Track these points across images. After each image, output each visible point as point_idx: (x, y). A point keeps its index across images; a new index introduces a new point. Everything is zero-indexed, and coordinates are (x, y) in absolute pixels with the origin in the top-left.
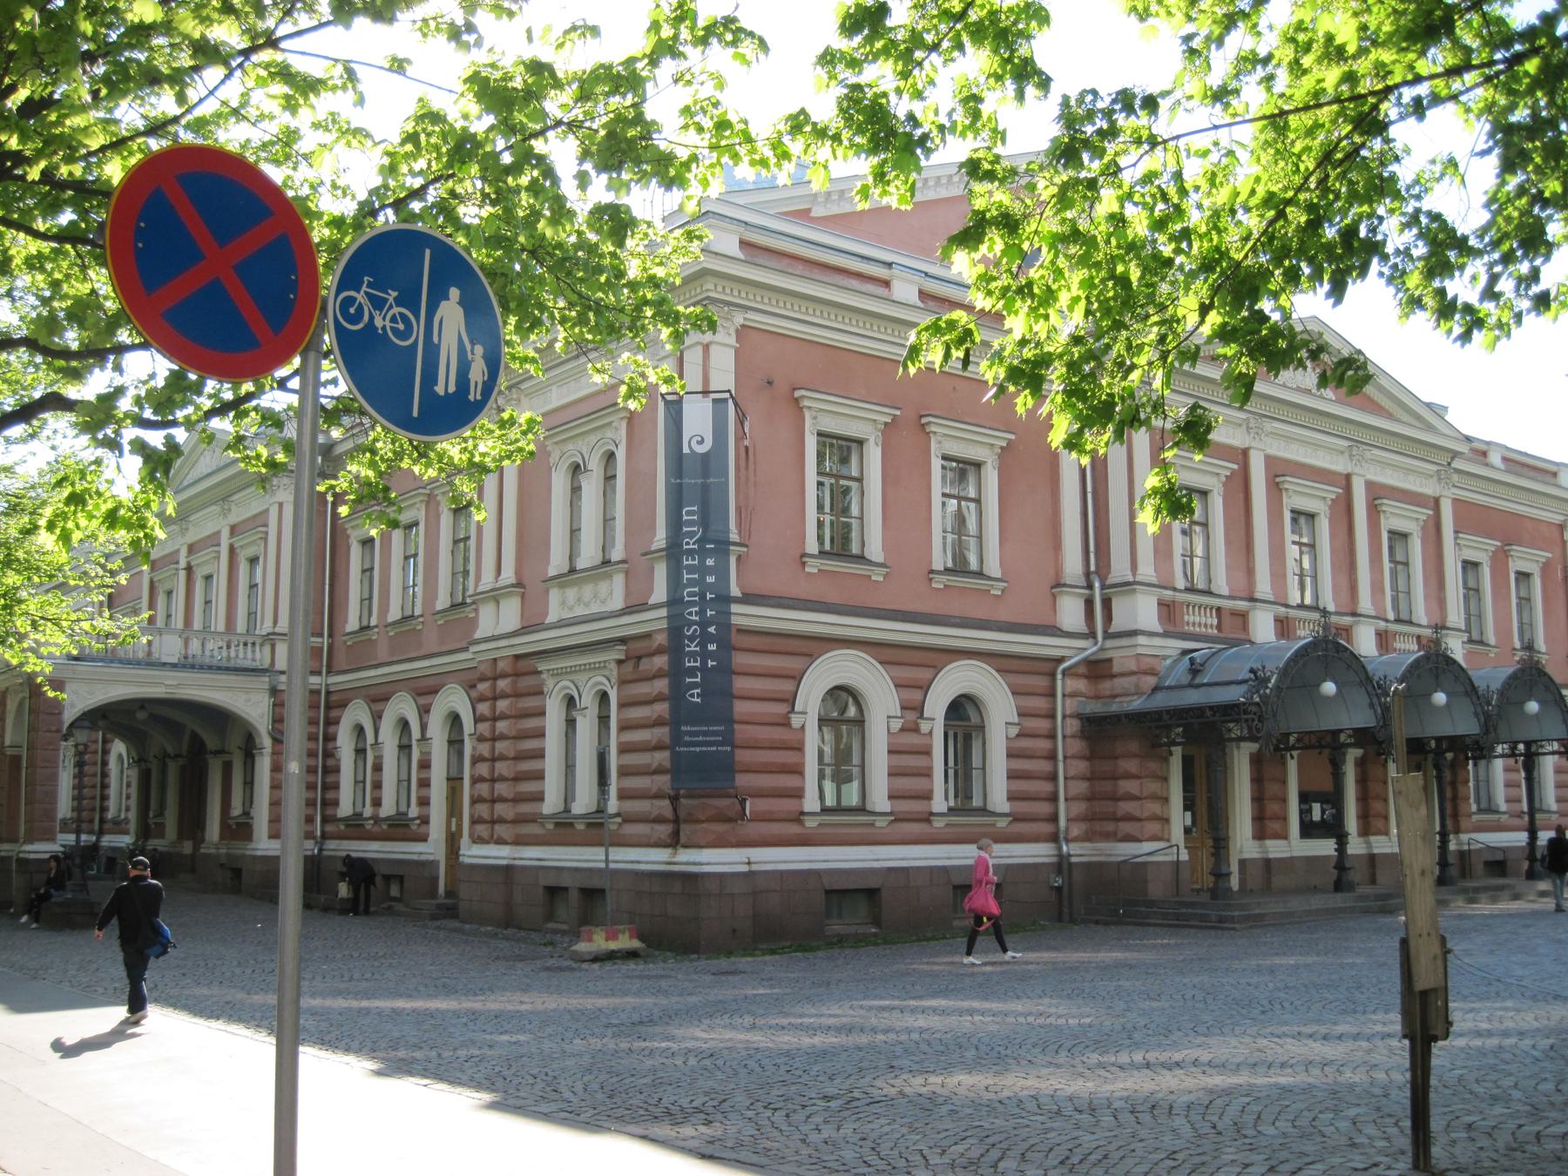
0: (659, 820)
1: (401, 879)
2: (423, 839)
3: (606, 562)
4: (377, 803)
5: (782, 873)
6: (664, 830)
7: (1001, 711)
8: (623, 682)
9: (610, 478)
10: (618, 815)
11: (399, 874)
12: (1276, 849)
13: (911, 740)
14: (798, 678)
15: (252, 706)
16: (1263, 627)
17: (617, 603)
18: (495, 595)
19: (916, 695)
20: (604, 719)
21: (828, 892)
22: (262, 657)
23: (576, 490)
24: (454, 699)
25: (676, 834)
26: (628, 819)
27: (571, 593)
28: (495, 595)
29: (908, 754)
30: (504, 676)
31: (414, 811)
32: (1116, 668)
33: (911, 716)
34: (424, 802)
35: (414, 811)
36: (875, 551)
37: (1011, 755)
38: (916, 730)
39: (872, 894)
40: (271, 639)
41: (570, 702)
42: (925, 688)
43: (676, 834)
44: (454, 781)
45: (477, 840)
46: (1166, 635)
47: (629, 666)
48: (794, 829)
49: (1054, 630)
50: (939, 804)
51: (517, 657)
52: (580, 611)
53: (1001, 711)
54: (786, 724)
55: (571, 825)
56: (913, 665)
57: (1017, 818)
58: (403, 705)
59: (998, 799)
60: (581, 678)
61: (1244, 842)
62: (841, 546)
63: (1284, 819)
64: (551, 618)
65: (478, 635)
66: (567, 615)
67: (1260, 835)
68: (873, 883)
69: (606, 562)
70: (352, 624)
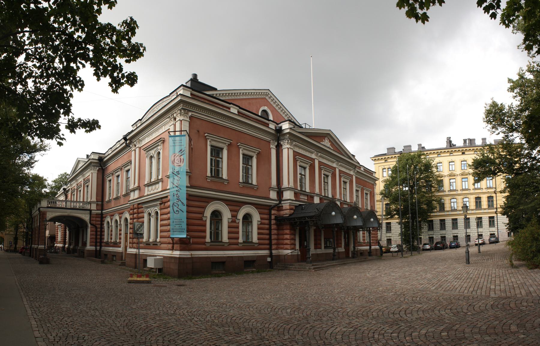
0: (169, 243)
1: (115, 256)
2: (120, 247)
3: (158, 179)
4: (111, 239)
5: (200, 257)
6: (170, 246)
7: (256, 218)
8: (161, 209)
9: (159, 159)
10: (160, 242)
11: (114, 254)
12: (319, 251)
13: (234, 224)
14: (204, 208)
15: (86, 217)
16: (317, 200)
17: (160, 189)
18: (134, 190)
19: (235, 213)
20: (157, 219)
21: (212, 262)
22: (88, 207)
23: (151, 163)
24: (127, 215)
25: (173, 247)
26: (161, 243)
27: (150, 188)
28: (134, 190)
29: (233, 227)
30: (136, 209)
31: (118, 241)
32: (284, 208)
33: (234, 218)
34: (120, 239)
35: (118, 241)
36: (225, 176)
37: (259, 229)
38: (235, 222)
39: (223, 263)
40: (90, 203)
41: (150, 214)
42: (237, 211)
43: (173, 247)
44: (126, 234)
45: (130, 248)
46: (296, 201)
47: (162, 205)
48: (203, 246)
49: (269, 198)
50: (241, 240)
51: (139, 204)
52: (152, 192)
53: (256, 218)
54: (201, 219)
55: (157, 244)
56: (235, 206)
57: (260, 244)
58: (117, 217)
59: (255, 239)
60: (152, 209)
61: (313, 250)
62: (216, 172)
63: (321, 244)
64: (146, 194)
65: (130, 199)
66: (149, 193)
67: (316, 248)
68: (224, 260)
69: (158, 179)
70: (107, 199)
